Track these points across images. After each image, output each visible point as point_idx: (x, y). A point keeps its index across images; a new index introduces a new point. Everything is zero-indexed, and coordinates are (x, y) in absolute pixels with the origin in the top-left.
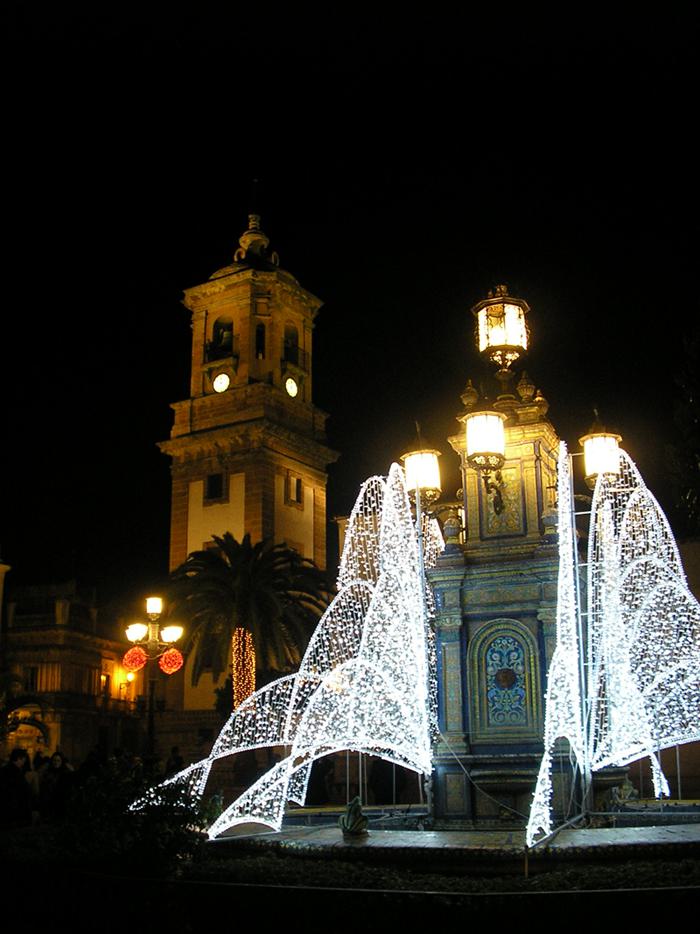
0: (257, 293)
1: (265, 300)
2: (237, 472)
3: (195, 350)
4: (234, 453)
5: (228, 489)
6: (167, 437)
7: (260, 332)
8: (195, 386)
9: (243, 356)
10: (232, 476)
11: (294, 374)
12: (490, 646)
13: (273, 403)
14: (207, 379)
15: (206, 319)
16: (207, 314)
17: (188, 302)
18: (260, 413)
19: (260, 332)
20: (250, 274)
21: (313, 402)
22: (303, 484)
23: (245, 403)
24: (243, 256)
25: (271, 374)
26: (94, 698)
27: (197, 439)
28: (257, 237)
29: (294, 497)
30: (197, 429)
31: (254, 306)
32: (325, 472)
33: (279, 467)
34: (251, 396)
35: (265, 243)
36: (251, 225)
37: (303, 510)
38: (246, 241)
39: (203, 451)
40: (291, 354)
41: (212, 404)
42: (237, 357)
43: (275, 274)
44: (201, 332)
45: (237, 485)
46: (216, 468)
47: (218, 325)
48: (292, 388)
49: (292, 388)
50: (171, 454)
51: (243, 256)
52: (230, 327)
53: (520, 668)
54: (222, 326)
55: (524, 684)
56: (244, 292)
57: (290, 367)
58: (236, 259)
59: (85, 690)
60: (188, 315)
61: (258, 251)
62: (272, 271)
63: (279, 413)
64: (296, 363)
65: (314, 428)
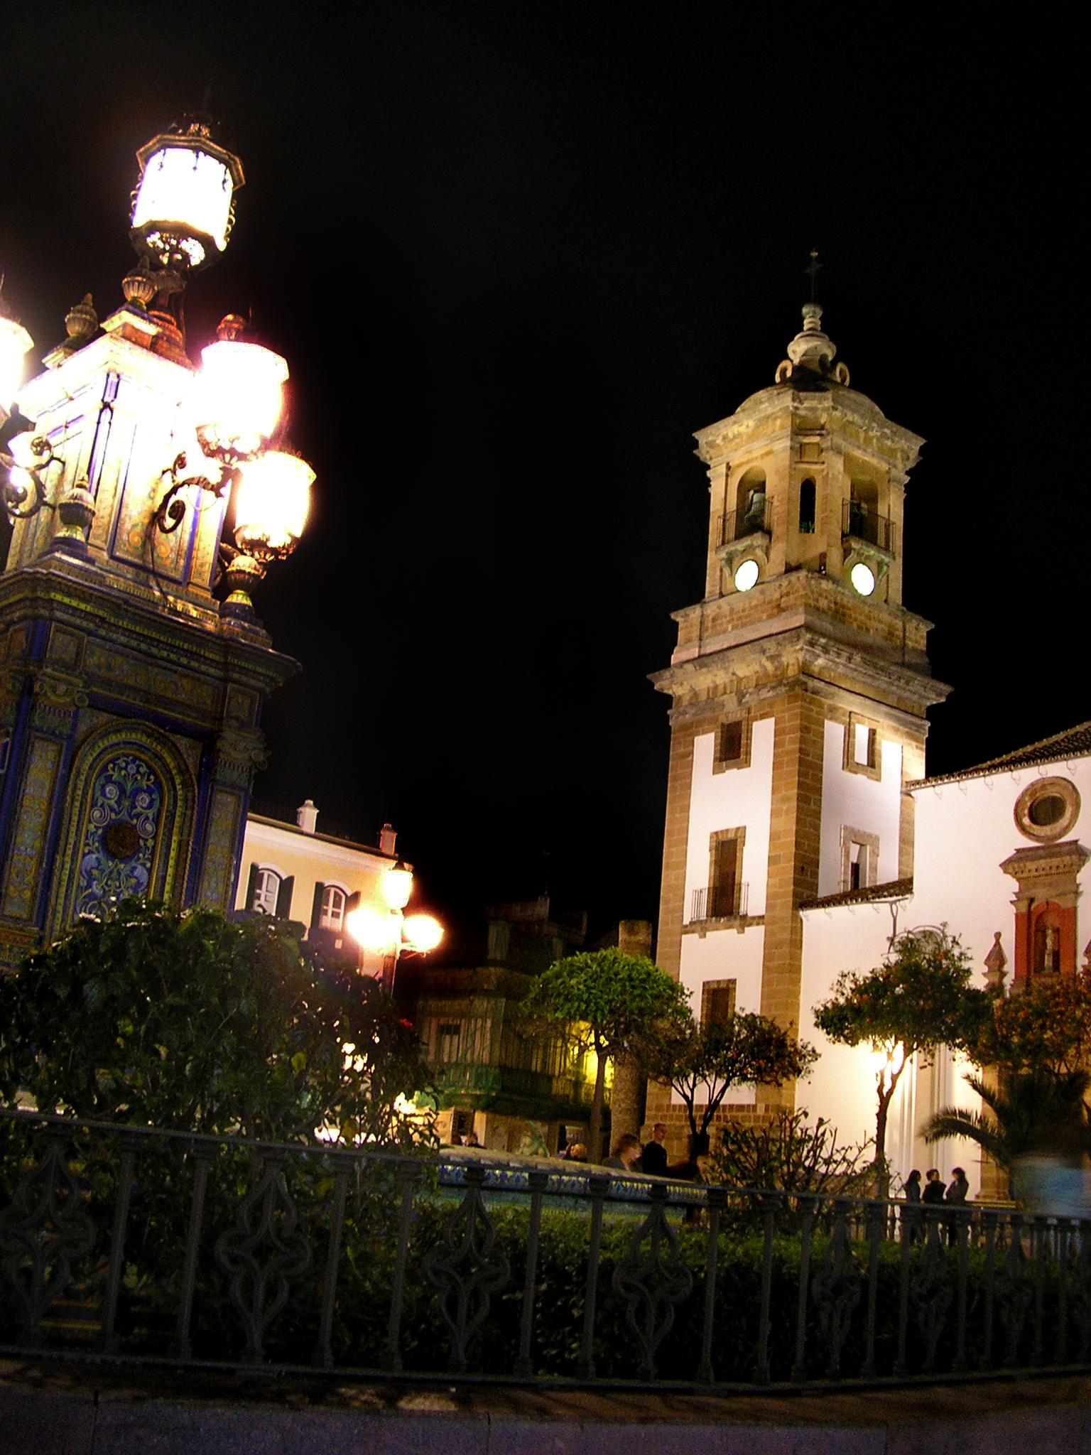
0: (801, 428)
1: (816, 439)
2: (762, 717)
3: (714, 525)
4: (758, 687)
5: (749, 745)
6: (666, 664)
7: (808, 489)
8: (711, 586)
9: (778, 530)
10: (755, 724)
11: (868, 557)
12: (105, 769)
13: (823, 603)
14: (727, 571)
15: (727, 476)
16: (729, 468)
17: (703, 453)
18: (799, 620)
19: (808, 489)
20: (790, 398)
21: (903, 604)
22: (878, 737)
23: (779, 606)
24: (789, 374)
25: (823, 556)
26: (550, 1078)
27: (706, 666)
28: (815, 343)
29: (861, 756)
30: (709, 650)
31: (799, 451)
32: (927, 719)
33: (833, 709)
34: (788, 594)
35: (830, 352)
36: (807, 324)
37: (878, 780)
38: (798, 349)
39: (716, 687)
40: (861, 526)
41: (732, 610)
42: (769, 533)
43: (829, 395)
44: (722, 495)
45: (763, 735)
46: (731, 710)
47: (744, 486)
48: (863, 579)
49: (863, 579)
50: (670, 692)
51: (789, 374)
52: (761, 487)
53: (149, 827)
54: (752, 485)
55: (152, 862)
56: (781, 426)
57: (855, 544)
58: (778, 379)
59: (536, 1065)
60: (698, 475)
61: (815, 366)
62: (824, 390)
63: (834, 624)
64: (872, 540)
65: (905, 645)
